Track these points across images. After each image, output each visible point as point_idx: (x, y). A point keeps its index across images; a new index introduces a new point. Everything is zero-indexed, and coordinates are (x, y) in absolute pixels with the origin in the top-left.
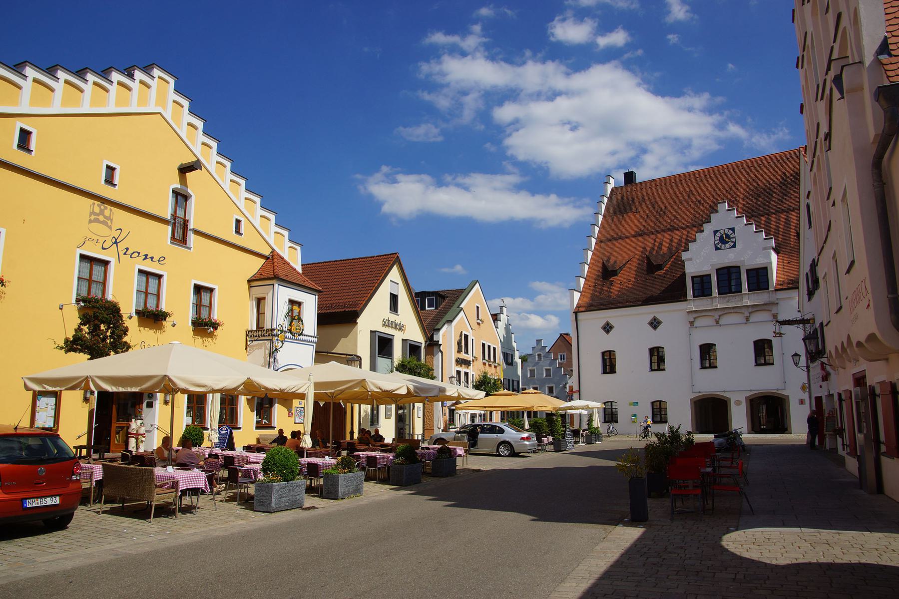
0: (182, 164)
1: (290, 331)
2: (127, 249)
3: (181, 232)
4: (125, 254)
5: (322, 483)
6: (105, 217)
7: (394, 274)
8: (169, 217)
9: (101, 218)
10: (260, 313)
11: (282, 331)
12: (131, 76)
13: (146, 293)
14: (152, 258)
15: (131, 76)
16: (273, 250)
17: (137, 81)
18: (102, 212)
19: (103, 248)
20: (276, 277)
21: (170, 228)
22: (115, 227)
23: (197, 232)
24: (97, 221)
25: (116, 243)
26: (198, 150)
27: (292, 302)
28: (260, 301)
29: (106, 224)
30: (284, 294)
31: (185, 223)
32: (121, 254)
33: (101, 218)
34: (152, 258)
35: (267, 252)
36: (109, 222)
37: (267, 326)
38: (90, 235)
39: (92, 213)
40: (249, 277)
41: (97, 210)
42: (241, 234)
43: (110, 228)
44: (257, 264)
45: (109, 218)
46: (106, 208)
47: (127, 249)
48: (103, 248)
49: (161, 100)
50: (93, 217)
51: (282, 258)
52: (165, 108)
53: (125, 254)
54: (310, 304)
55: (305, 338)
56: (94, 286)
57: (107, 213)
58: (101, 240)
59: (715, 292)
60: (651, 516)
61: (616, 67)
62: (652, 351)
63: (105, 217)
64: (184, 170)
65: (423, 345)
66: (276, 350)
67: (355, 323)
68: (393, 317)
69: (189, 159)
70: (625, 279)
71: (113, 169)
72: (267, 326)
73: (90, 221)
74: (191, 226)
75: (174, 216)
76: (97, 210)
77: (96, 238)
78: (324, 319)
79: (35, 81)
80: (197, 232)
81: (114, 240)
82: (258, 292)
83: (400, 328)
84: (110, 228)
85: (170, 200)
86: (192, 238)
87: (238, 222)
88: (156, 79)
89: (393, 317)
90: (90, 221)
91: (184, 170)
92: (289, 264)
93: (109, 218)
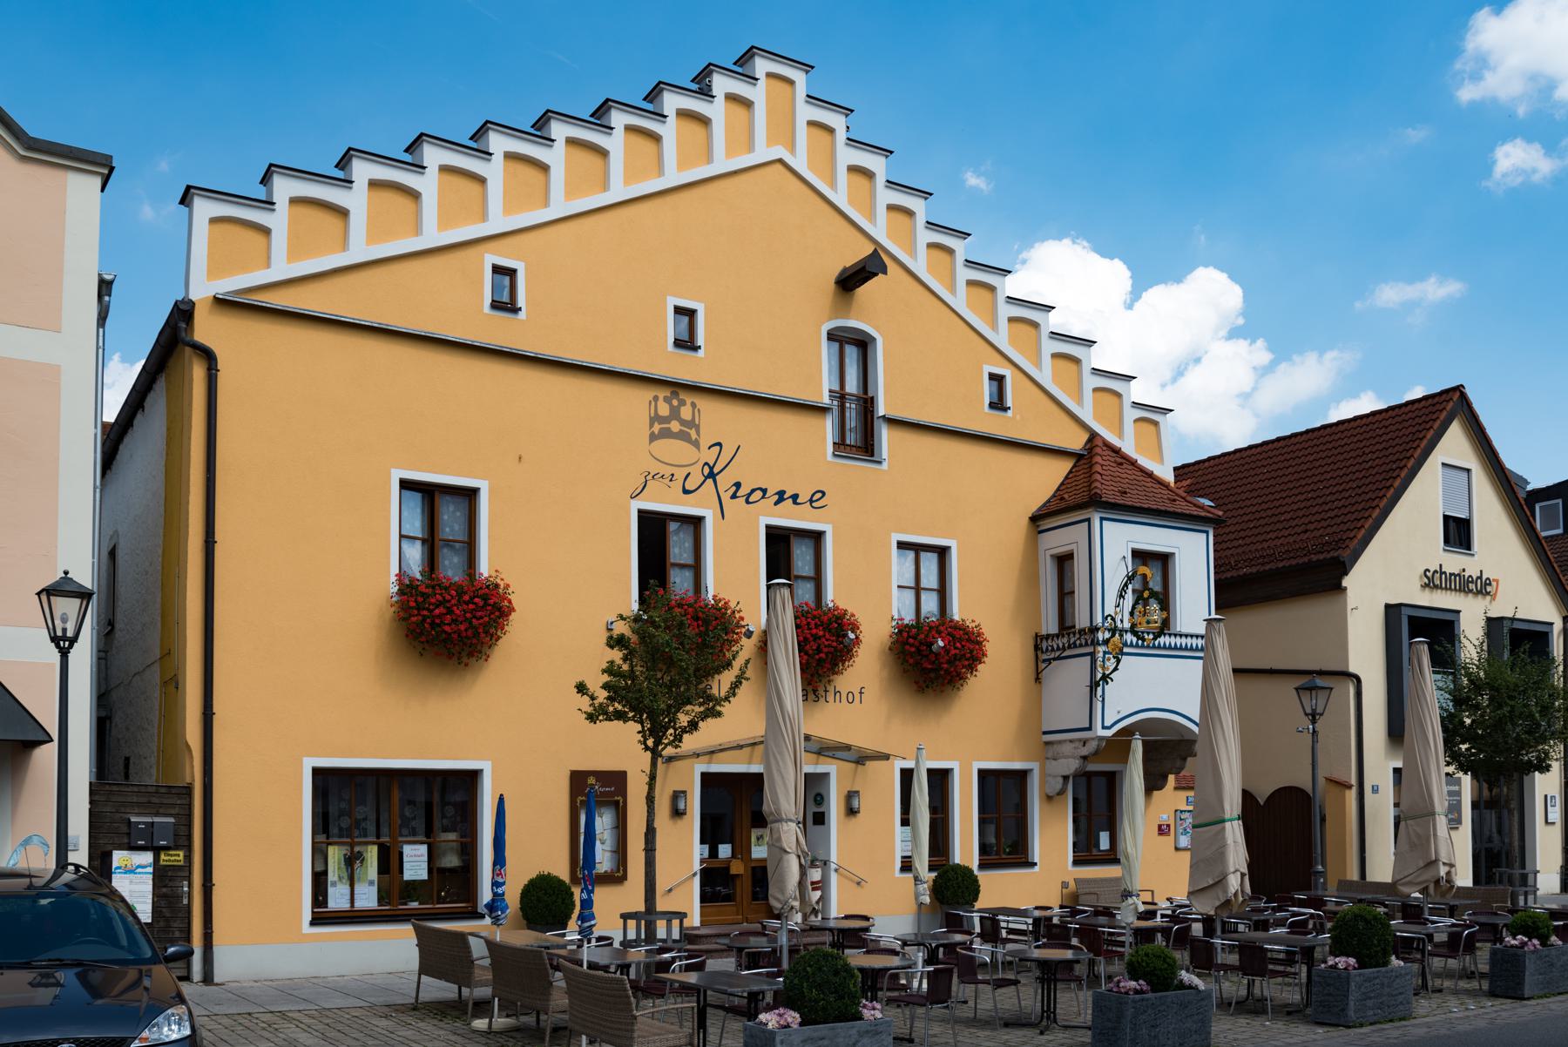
0: (845, 270)
1: (1133, 630)
3: (860, 431)
4: (734, 496)
5: (452, 836)
6: (683, 422)
7: (1454, 445)
8: (826, 400)
9: (675, 426)
10: (1065, 595)
11: (1113, 631)
12: (705, 92)
13: (918, 589)
14: (795, 497)
15: (705, 92)
16: (1093, 436)
17: (720, 99)
18: (675, 414)
19: (686, 492)
20: (1095, 502)
22: (705, 442)
23: (893, 422)
24: (666, 434)
25: (712, 475)
26: (880, 230)
27: (1140, 556)
28: (1064, 561)
30: (1117, 542)
31: (867, 404)
32: (726, 497)
33: (675, 426)
34: (795, 497)
35: (1077, 442)
36: (693, 433)
37: (1082, 622)
38: (655, 468)
39: (655, 418)
40: (1034, 505)
41: (664, 410)
42: (1006, 409)
43: (696, 444)
44: (1048, 476)
45: (692, 424)
46: (682, 403)
47: (738, 485)
48: (686, 492)
49: (784, 131)
50: (657, 428)
51: (1117, 451)
52: (792, 148)
53: (734, 496)
54: (1193, 557)
55: (1173, 641)
56: (924, 596)
57: (686, 413)
58: (680, 474)
63: (683, 422)
64: (851, 280)
65: (1558, 626)
66: (1105, 678)
67: (1339, 589)
68: (1454, 562)
69: (858, 252)
71: (690, 313)
72: (1082, 622)
73: (653, 438)
74: (881, 410)
75: (841, 396)
76: (664, 410)
77: (667, 471)
78: (1233, 591)
79: (510, 156)
80: (893, 422)
81: (706, 470)
82: (1058, 541)
83: (1481, 587)
84: (696, 444)
85: (825, 353)
86: (886, 437)
87: (998, 379)
88: (762, 83)
89: (1454, 562)
90: (653, 438)
91: (851, 280)
92: (1133, 463)
93: (692, 424)
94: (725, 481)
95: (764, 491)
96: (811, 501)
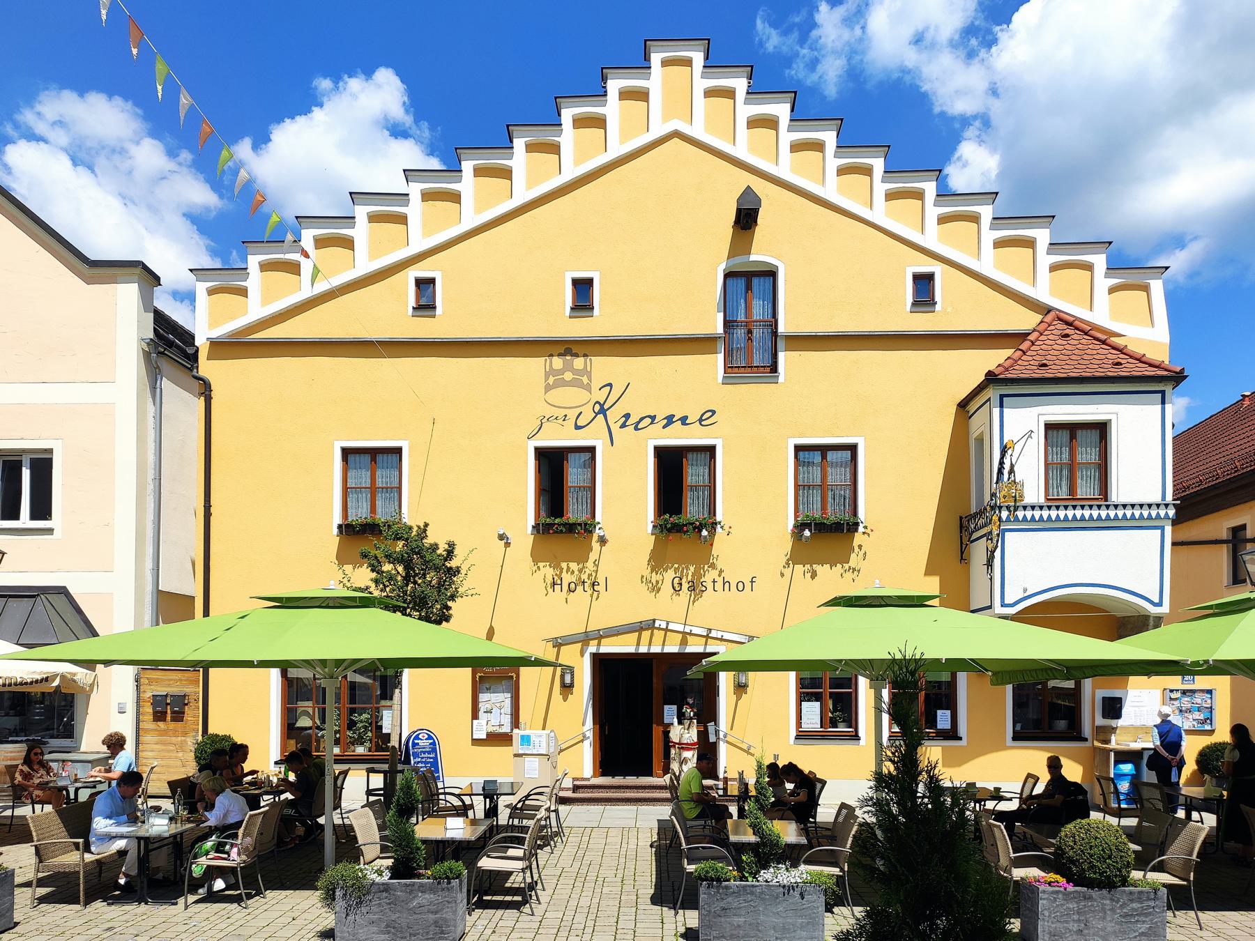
2: (627, 416)
4: (623, 426)
21: (781, 329)
22: (596, 385)
25: (603, 411)
29: (579, 384)
32: (615, 428)
38: (550, 411)
43: (588, 388)
47: (627, 416)
50: (551, 380)
53: (623, 426)
58: (572, 414)
59: (169, 718)
60: (701, 903)
61: (137, 115)
62: (1029, 776)
63: (575, 372)
70: (293, 673)
73: (548, 388)
81: (597, 408)
84: (588, 388)
90: (548, 388)
94: (614, 415)
95: (653, 418)
96: (701, 420)
